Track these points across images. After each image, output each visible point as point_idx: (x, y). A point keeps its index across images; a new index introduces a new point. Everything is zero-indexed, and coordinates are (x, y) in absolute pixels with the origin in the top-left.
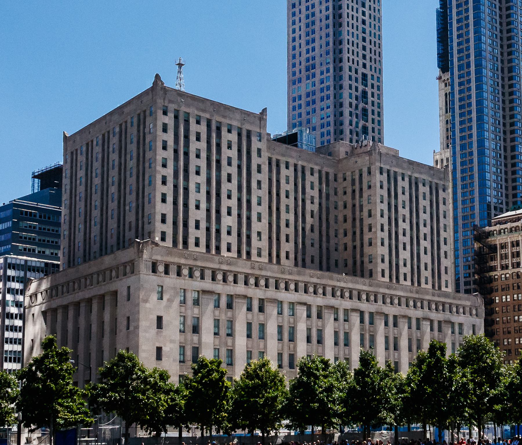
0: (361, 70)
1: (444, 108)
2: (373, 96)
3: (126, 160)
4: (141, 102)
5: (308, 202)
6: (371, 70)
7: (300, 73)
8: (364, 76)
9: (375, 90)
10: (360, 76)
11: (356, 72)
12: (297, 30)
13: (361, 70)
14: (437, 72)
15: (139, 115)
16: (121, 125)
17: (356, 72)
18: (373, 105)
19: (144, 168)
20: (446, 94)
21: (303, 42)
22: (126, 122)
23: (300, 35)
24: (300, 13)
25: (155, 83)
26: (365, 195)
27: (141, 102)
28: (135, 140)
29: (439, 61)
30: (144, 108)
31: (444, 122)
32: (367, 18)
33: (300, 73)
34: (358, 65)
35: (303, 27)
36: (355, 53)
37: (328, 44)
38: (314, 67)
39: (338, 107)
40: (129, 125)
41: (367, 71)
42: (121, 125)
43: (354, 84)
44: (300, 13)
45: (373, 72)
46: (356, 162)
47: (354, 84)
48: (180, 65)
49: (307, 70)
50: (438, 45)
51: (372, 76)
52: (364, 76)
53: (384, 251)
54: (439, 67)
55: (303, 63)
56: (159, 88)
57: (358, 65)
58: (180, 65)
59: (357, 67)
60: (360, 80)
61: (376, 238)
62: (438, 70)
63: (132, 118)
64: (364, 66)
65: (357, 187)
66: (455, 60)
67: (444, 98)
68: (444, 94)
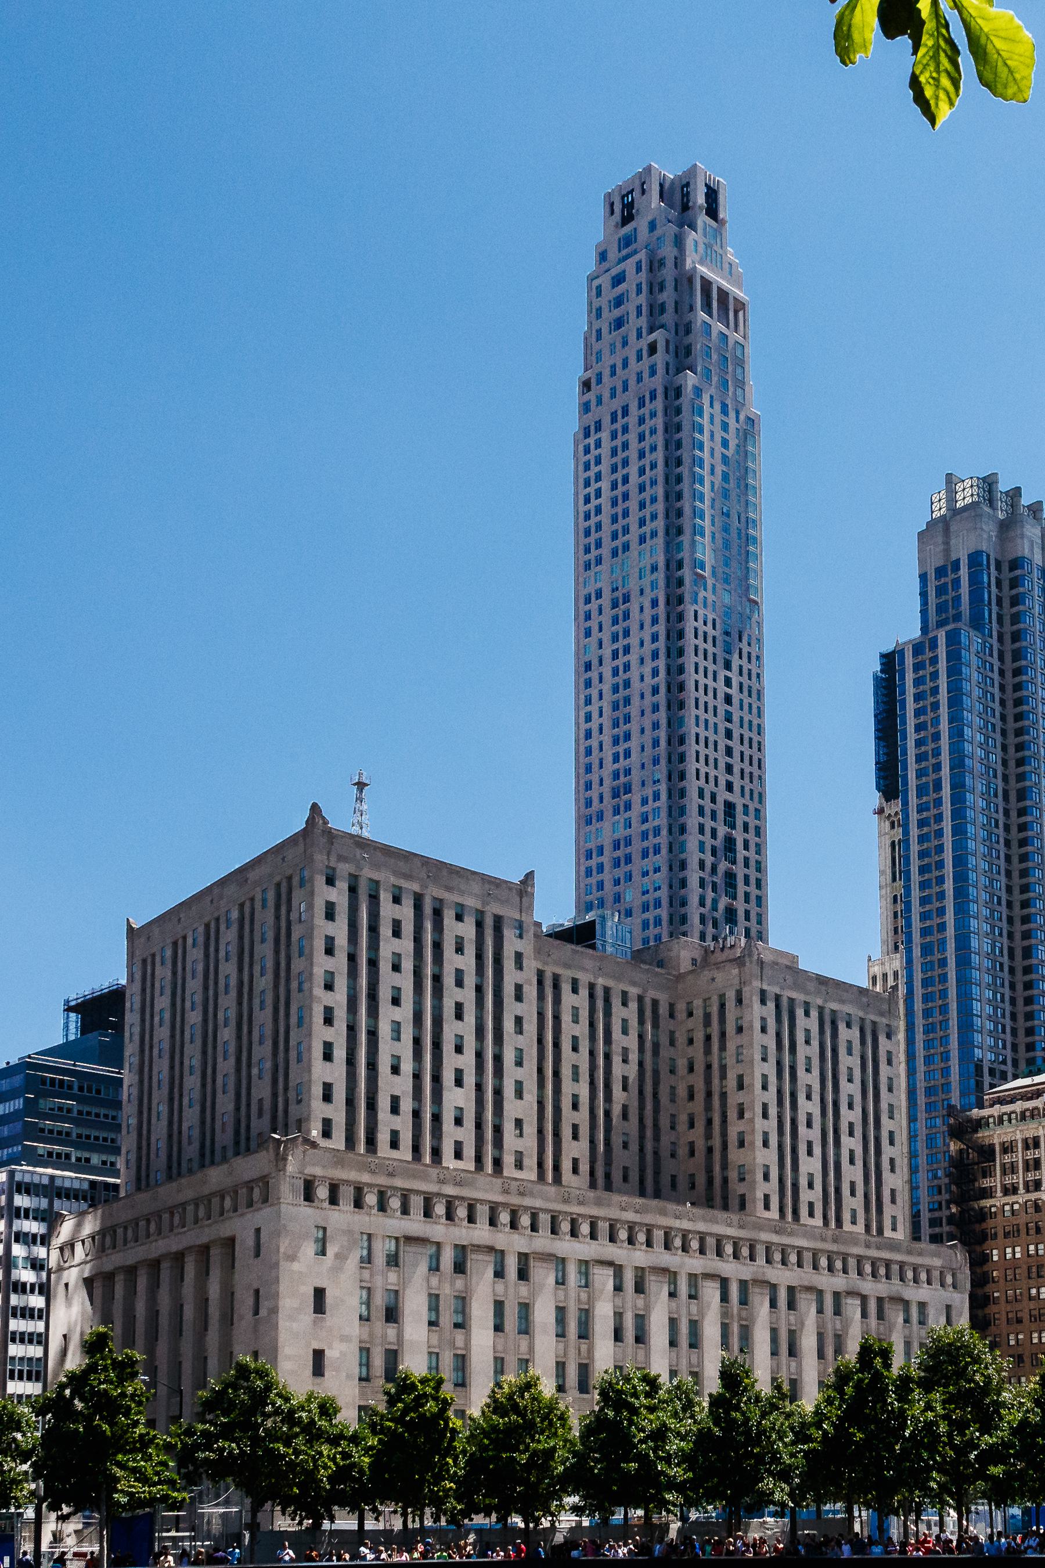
0: (723, 795)
1: (889, 872)
2: (746, 847)
3: (251, 976)
4: (283, 859)
5: (617, 1060)
6: (743, 795)
7: (601, 801)
8: (730, 807)
9: (751, 836)
10: (720, 807)
11: (713, 800)
12: (595, 715)
13: (723, 795)
14: (875, 799)
15: (278, 885)
16: (242, 906)
17: (713, 800)
18: (747, 865)
19: (288, 991)
20: (893, 843)
21: (607, 739)
22: (252, 899)
23: (601, 725)
24: (601, 681)
25: (311, 822)
26: (731, 1046)
27: (283, 859)
28: (270, 935)
29: (878, 778)
30: (289, 872)
31: (890, 900)
32: (734, 691)
33: (601, 801)
34: (716, 785)
35: (607, 710)
36: (711, 761)
37: (656, 743)
38: (628, 789)
39: (676, 868)
40: (258, 905)
41: (735, 798)
42: (242, 906)
43: (709, 824)
44: (601, 681)
45: (747, 800)
46: (713, 979)
47: (709, 824)
48: (361, 785)
49: (616, 794)
50: (877, 745)
51: (745, 806)
52: (730, 807)
53: (768, 1157)
54: (878, 789)
55: (608, 696)
56: (318, 831)
57: (716, 785)
58: (361, 785)
59: (714, 790)
60: (721, 815)
61: (753, 1131)
62: (878, 794)
63: (264, 891)
64: (729, 787)
65: (715, 1030)
66: (912, 775)
67: (889, 850)
68: (888, 843)
